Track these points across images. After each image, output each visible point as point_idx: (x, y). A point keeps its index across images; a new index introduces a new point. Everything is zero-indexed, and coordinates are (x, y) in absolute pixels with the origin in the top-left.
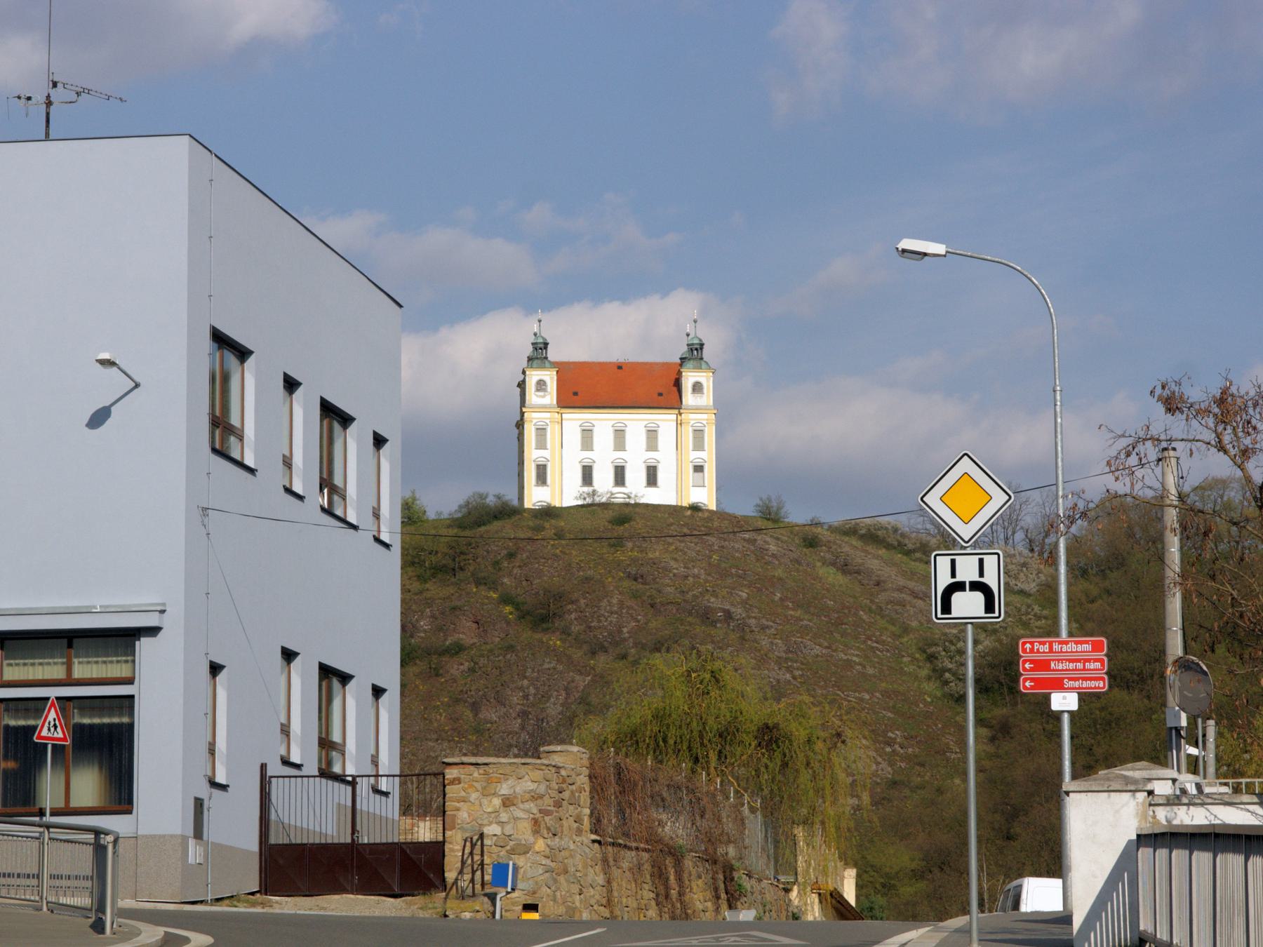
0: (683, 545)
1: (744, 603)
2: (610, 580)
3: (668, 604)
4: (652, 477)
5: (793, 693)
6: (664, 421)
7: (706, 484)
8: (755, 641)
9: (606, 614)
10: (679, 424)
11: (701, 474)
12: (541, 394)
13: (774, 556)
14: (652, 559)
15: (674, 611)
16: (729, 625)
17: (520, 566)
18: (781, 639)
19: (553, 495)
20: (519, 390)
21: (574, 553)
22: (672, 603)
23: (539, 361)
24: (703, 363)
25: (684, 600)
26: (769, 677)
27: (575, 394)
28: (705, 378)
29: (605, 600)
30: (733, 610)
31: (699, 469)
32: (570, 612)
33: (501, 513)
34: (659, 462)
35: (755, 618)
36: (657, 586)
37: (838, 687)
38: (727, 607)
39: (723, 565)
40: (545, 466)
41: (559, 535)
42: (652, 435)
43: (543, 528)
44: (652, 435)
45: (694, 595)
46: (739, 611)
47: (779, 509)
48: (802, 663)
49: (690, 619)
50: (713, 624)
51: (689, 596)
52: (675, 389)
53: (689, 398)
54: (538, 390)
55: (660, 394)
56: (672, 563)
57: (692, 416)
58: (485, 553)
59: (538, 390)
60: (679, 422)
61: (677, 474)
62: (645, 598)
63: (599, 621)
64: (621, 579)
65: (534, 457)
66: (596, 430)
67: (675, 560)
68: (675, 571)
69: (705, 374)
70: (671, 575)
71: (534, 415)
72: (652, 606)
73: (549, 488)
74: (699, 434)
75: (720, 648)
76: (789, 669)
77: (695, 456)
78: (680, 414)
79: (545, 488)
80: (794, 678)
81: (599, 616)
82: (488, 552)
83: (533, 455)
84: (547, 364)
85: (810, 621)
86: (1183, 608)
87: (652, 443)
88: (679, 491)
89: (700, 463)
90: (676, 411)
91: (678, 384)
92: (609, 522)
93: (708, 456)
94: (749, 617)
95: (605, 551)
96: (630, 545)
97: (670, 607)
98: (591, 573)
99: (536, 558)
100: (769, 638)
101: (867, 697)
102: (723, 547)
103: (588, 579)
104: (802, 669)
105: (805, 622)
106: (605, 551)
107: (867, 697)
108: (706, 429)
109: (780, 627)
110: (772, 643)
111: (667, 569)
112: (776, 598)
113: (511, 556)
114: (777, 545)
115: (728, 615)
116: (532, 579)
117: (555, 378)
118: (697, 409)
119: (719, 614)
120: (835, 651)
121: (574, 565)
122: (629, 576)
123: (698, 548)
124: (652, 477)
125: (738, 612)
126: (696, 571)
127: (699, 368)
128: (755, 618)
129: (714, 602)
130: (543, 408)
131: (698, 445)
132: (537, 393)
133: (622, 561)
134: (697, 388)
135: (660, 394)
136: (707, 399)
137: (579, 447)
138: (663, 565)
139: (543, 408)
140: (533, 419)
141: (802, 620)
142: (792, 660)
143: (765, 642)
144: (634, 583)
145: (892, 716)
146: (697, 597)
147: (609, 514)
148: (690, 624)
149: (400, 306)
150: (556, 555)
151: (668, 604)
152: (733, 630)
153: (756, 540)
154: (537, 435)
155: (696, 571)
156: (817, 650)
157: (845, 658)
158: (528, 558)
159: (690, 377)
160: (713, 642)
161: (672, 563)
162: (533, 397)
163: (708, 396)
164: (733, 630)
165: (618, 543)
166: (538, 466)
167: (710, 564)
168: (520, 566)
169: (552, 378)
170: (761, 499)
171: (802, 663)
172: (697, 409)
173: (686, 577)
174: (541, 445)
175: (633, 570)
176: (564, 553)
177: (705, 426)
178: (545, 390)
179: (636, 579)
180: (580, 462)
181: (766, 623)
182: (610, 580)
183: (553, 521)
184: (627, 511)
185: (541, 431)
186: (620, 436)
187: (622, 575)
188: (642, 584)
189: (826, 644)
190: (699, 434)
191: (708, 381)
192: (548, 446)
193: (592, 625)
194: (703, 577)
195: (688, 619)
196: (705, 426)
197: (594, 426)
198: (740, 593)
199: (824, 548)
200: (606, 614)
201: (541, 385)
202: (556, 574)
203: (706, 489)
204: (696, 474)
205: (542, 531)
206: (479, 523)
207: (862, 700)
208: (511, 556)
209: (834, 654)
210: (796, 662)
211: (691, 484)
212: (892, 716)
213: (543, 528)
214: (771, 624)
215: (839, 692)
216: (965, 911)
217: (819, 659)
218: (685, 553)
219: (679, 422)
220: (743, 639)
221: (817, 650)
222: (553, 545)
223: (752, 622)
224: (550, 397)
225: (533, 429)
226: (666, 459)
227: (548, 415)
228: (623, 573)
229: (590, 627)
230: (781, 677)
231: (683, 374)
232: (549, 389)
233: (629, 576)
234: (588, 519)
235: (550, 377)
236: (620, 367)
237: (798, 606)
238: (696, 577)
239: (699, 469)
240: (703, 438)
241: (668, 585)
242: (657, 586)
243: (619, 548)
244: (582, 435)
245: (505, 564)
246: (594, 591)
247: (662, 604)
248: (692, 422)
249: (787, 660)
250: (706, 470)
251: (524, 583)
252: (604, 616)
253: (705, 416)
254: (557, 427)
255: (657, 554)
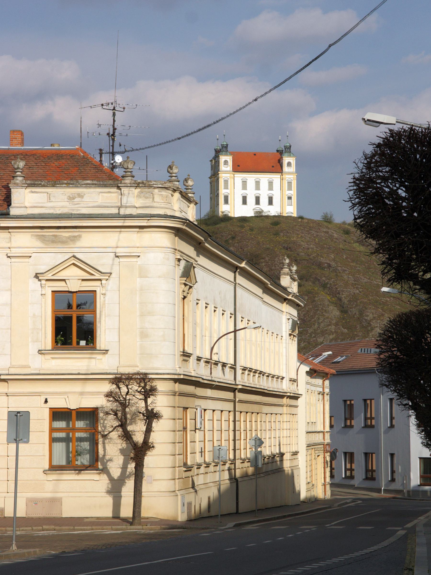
0: (303, 235)
1: (334, 260)
2: (276, 249)
3: (303, 260)
4: (271, 202)
5: (361, 298)
6: (276, 178)
7: (293, 205)
8: (342, 276)
9: (278, 264)
10: (282, 179)
11: (290, 200)
12: (226, 166)
13: (336, 239)
14: (293, 241)
15: (306, 263)
16: (330, 269)
17: (237, 243)
18: (351, 275)
19: (231, 208)
20: (210, 162)
21: (259, 237)
22: (304, 260)
23: (225, 152)
24: (291, 154)
25: (310, 259)
26: (351, 292)
27: (239, 166)
28: (292, 160)
29: (277, 258)
30: (331, 263)
31: (290, 198)
32: (262, 263)
33: (224, 219)
34: (273, 195)
35: (340, 266)
36: (296, 252)
37: (377, 295)
38: (329, 262)
39: (321, 243)
40: (227, 196)
41: (252, 230)
42: (271, 184)
43: (244, 227)
44: (271, 184)
45: (313, 257)
46: (334, 264)
47: (331, 217)
48: (362, 286)
49: (313, 267)
50: (323, 269)
51: (311, 257)
52: (279, 164)
53: (286, 169)
54: (224, 164)
55: (273, 167)
56: (302, 243)
57: (287, 176)
58: (221, 237)
59: (224, 164)
60: (282, 178)
61: (281, 201)
62: (292, 257)
63: (275, 267)
64: (281, 249)
65: (223, 192)
66: (248, 181)
67: (303, 241)
68: (304, 246)
69: (292, 159)
70: (302, 248)
71: (223, 175)
72: (296, 261)
73: (229, 205)
74: (290, 183)
75: (328, 279)
76: (357, 288)
77: (288, 193)
78: (282, 175)
79: (228, 205)
80: (360, 292)
81: (275, 265)
82: (222, 236)
83: (222, 191)
84: (228, 154)
85: (359, 267)
86: (228, 186)
87: (271, 187)
88: (282, 206)
89: (290, 195)
90: (280, 174)
91: (280, 162)
92: (271, 224)
93: (293, 193)
94: (338, 266)
95: (272, 237)
96: (282, 234)
97: (303, 261)
98: (268, 246)
99: (244, 239)
100: (347, 275)
101: (389, 300)
102: (317, 235)
103: (268, 249)
104: (362, 288)
105: (358, 268)
106: (272, 237)
107: (389, 300)
108: (293, 182)
109: (350, 271)
110: (348, 277)
111: (300, 245)
112: (344, 258)
113: (233, 238)
114: (336, 234)
115: (329, 266)
116: (243, 248)
117: (232, 159)
118: (289, 173)
119: (326, 265)
120: (372, 280)
121: (261, 243)
122: (284, 247)
123: (309, 236)
124: (271, 202)
125: (333, 264)
126: (312, 246)
127: (290, 156)
128: (340, 266)
129: (322, 260)
130: (226, 172)
131: (290, 188)
132: (225, 166)
133: (281, 241)
134: (289, 164)
135: (273, 167)
136: (293, 169)
137: (254, 188)
138: (298, 243)
139: (226, 172)
140: (222, 177)
141: (357, 267)
142: (357, 285)
143: (345, 277)
144: (287, 250)
145: (399, 308)
146: (315, 257)
147: (270, 221)
148: (314, 269)
149: (377, 136)
150: (253, 238)
151: (303, 260)
152: (332, 272)
153: (328, 232)
154: (224, 183)
155: (312, 246)
156: (366, 280)
157: (376, 283)
158: (240, 239)
159: (286, 160)
160: (325, 277)
161: (302, 243)
162: (222, 167)
163: (293, 168)
164: (332, 272)
165: (277, 234)
166: (225, 196)
167: (315, 243)
168: (237, 243)
169: (230, 160)
170: (324, 213)
171: (362, 286)
172: (289, 173)
173: (308, 249)
174: (226, 187)
175: (286, 246)
176: (255, 237)
177: (292, 180)
178: (228, 165)
179: (287, 249)
180: (241, 195)
181: (344, 268)
182: (276, 249)
183: (247, 223)
184: (276, 219)
185: (226, 182)
186: (258, 184)
187: (281, 247)
188: (290, 251)
189: (368, 277)
190: (290, 183)
191: (293, 162)
192: (293, 190)
193: (273, 268)
194: (315, 248)
195: (312, 267)
196: (292, 180)
197: (247, 180)
198: (331, 256)
199: (352, 234)
200: (278, 264)
201: (226, 162)
202: (254, 246)
203: (292, 206)
204: (289, 200)
205: (244, 228)
206: (215, 223)
207: (387, 301)
208: (233, 238)
209: (372, 282)
210: (359, 285)
211: (287, 204)
212: (399, 308)
213: (244, 227)
214: (346, 269)
215: (378, 298)
216: (17, 536)
217: (367, 284)
218: (305, 238)
219: (282, 178)
220: (337, 275)
221: (366, 280)
222: (250, 234)
223: (339, 268)
224: (230, 168)
225: (223, 181)
226: (276, 194)
227: (229, 175)
228: (281, 246)
229: (272, 269)
230: (355, 292)
231: (284, 158)
232: (229, 164)
233: (284, 247)
234: (261, 223)
235: (229, 159)
236: (255, 155)
237: (353, 261)
238: (313, 249)
239: (290, 198)
240: (291, 185)
241: (301, 252)
242: (296, 252)
243: (278, 236)
244: (243, 183)
245: (231, 241)
246: (271, 254)
247: (300, 260)
248: (287, 179)
249: (355, 284)
250: (293, 198)
251: (240, 250)
252: (277, 265)
253: (292, 176)
254: (233, 180)
255: (295, 238)
